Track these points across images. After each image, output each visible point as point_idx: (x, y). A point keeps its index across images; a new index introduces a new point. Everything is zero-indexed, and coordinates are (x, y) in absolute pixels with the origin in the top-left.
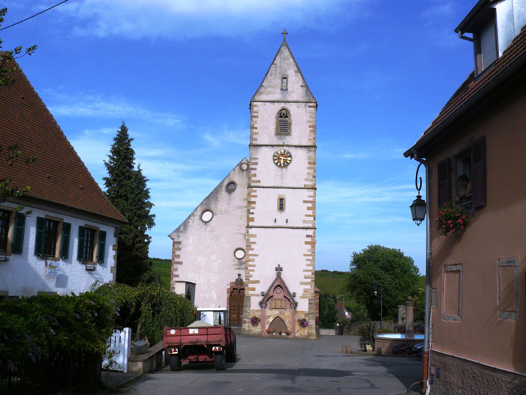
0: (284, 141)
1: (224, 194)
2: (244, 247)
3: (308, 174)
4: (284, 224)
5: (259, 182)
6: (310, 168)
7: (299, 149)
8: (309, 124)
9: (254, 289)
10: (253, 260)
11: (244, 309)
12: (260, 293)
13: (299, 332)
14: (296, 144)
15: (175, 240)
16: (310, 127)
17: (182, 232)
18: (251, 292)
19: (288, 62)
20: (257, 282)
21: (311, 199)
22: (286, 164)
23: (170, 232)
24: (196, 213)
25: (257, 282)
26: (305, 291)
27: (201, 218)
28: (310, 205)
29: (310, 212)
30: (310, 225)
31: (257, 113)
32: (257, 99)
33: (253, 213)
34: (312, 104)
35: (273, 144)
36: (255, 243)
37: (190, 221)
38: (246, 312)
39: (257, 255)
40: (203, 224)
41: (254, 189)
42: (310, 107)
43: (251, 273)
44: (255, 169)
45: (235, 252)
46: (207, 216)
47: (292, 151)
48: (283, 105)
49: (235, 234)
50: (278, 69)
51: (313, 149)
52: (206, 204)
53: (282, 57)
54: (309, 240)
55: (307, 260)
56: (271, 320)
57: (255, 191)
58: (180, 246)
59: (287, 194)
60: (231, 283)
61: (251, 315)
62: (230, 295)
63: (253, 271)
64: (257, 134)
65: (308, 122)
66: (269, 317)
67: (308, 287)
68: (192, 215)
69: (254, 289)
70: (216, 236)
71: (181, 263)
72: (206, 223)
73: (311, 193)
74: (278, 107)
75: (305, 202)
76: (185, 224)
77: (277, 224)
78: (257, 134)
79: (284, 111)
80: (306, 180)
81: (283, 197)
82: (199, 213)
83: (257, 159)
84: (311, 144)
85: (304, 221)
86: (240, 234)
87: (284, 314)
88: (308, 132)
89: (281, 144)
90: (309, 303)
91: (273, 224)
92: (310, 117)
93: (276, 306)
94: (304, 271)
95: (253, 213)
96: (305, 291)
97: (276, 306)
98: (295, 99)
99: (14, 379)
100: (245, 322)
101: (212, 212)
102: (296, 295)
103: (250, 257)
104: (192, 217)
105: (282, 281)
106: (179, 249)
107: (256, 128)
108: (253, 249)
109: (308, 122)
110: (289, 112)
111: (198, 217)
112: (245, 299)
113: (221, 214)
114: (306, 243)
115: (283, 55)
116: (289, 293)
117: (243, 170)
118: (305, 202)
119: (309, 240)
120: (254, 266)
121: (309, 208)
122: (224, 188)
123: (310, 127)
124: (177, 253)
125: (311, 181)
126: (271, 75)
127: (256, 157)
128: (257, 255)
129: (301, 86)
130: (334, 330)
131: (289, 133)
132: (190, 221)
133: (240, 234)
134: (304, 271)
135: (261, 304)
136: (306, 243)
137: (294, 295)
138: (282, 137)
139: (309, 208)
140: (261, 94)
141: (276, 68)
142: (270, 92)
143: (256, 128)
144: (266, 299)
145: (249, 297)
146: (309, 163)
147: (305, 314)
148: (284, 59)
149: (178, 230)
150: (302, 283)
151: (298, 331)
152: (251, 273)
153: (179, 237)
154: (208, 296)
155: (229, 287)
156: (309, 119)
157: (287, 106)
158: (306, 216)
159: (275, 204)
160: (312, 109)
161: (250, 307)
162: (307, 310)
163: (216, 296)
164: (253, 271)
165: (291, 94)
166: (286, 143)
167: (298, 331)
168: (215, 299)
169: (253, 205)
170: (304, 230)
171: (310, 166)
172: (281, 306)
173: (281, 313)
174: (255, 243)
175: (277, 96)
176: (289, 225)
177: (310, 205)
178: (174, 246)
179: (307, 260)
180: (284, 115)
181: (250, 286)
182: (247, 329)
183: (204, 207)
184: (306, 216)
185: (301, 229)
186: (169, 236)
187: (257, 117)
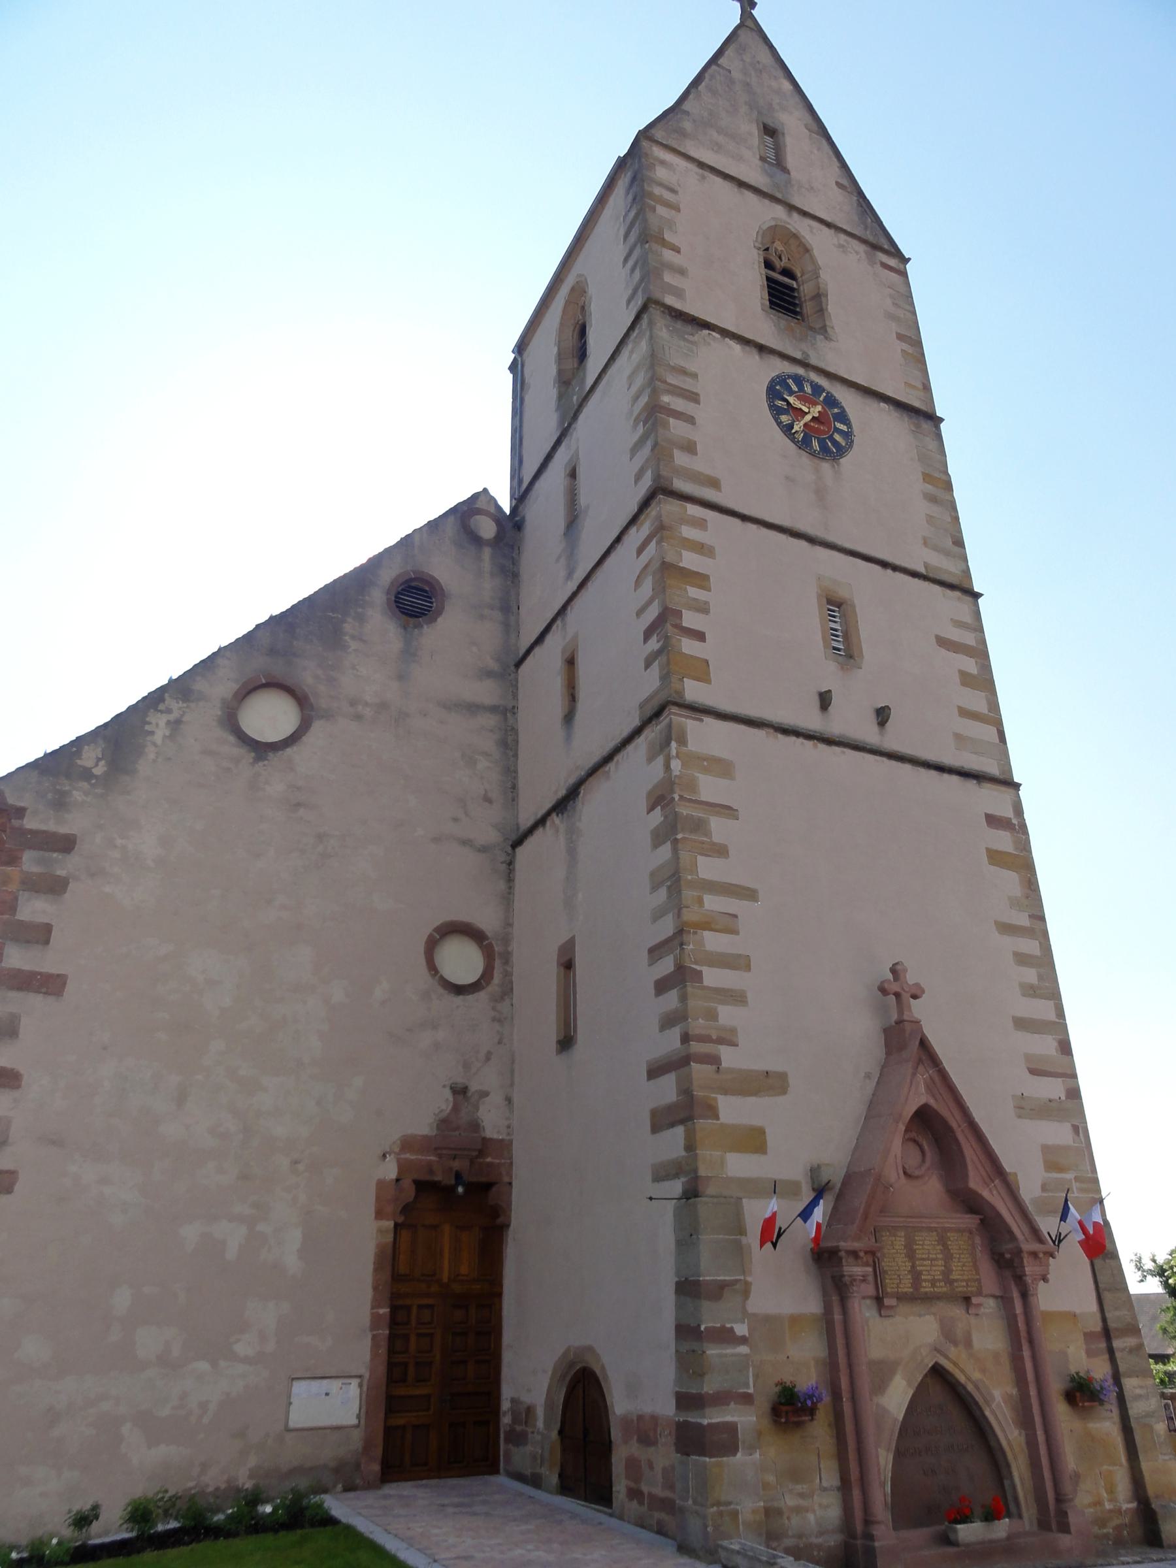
1: (378, 623)
2: (487, 919)
4: (869, 733)
9: (753, 1140)
18: (739, 1165)
20: (770, 1083)
25: (770, 1083)
27: (231, 722)
36: (728, 811)
41: (693, 510)
43: (727, 1015)
45: (431, 946)
46: (270, 717)
49: (436, 840)
52: (272, 652)
55: (41, 935)
57: (701, 524)
60: (407, 1144)
63: (737, 998)
69: (753, 1140)
70: (320, 837)
71: (51, 985)
72: (261, 750)
82: (223, 687)
86: (465, 842)
87: (968, 1343)
91: (812, 720)
101: (301, 699)
103: (713, 903)
108: (721, 851)
111: (214, 711)
113: (358, 717)
117: (476, 540)
120: (739, 963)
122: (378, 597)
127: (692, 367)
128: (750, 894)
133: (465, 842)
152: (727, 1015)
153: (60, 803)
154: (233, 1236)
155: (390, 1170)
163: (295, 1238)
164: (737, 998)
166: (813, 361)
168: (292, 1262)
169: (693, 592)
173: (947, 1332)
174: (728, 811)
176: (891, 742)
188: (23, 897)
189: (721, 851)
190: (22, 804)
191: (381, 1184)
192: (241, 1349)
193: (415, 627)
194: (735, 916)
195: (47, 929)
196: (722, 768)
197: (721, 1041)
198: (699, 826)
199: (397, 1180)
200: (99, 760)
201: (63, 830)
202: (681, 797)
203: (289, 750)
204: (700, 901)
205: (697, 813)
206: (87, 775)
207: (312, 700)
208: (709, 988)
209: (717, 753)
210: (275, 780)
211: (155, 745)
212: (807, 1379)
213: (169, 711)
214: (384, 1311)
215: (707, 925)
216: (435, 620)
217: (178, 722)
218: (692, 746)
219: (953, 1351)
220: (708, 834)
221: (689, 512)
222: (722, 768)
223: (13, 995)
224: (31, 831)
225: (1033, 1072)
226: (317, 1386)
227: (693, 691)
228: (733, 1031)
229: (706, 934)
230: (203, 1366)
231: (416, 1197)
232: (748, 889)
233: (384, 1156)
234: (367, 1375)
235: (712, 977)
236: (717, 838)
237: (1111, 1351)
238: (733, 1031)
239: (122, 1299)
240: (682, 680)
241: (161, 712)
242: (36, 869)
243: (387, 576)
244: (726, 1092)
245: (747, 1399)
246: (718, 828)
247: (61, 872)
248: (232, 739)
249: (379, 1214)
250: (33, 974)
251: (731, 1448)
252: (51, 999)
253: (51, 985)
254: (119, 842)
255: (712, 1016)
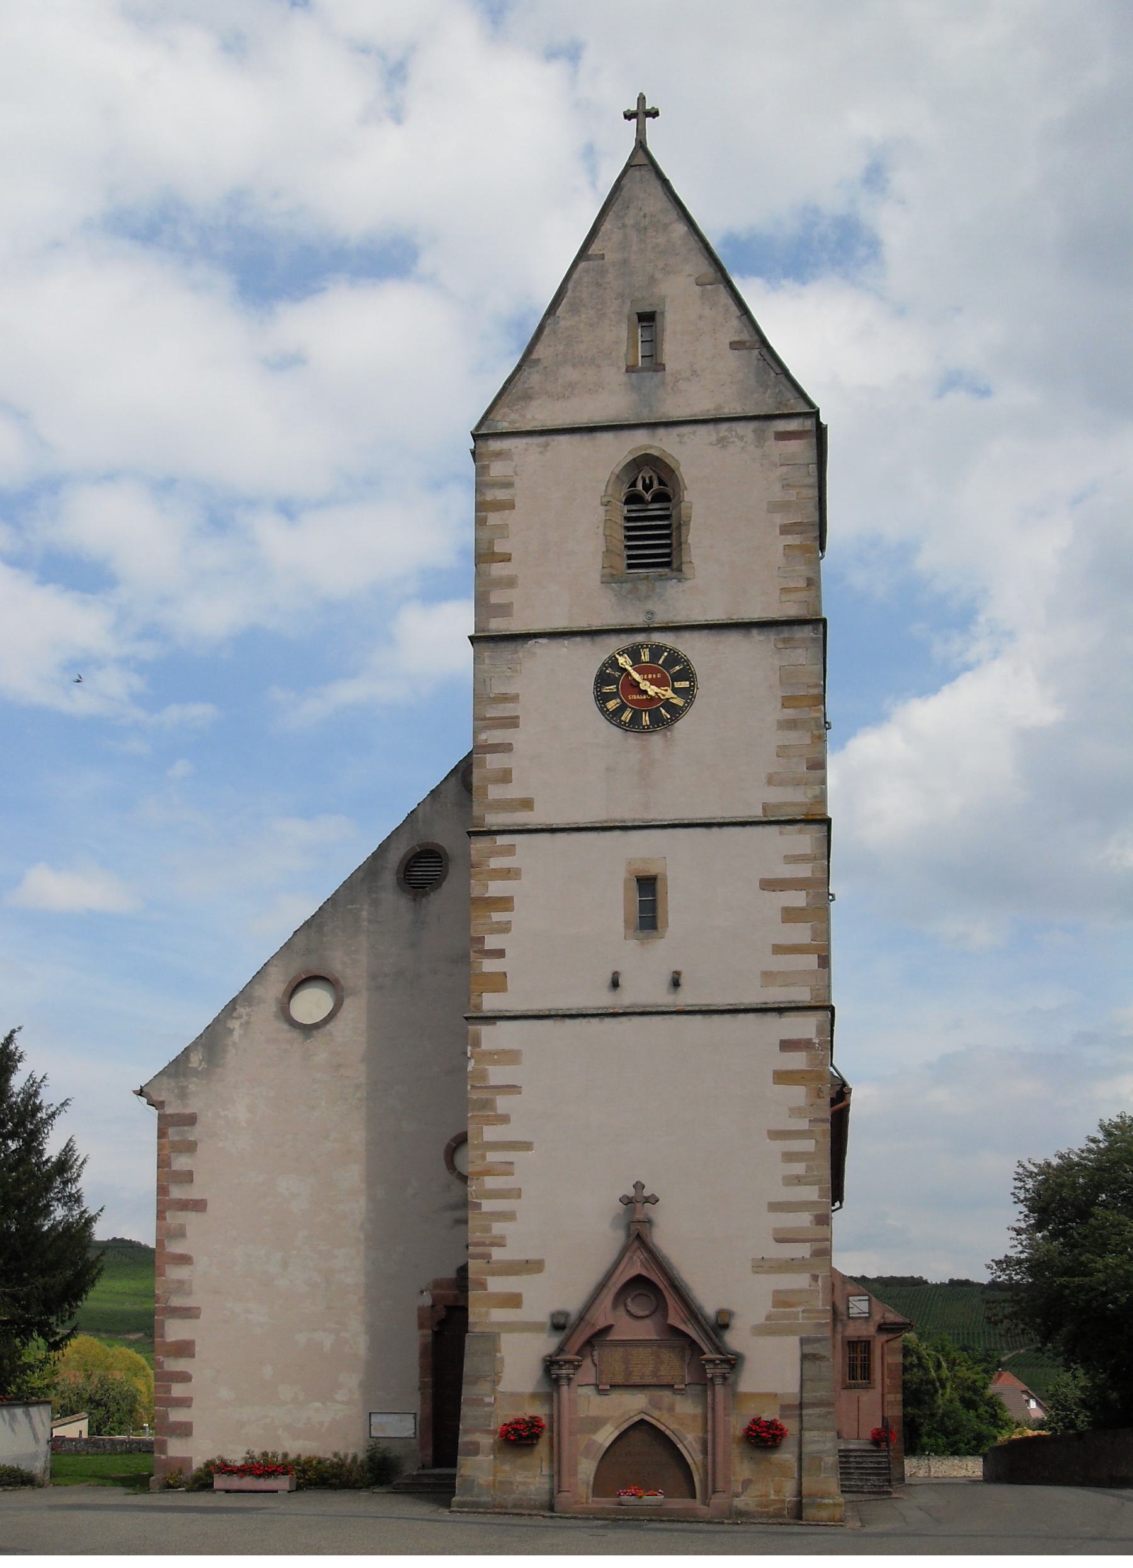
0: (650, 606)
3: (783, 751)
4: (663, 997)
5: (527, 804)
6: (790, 725)
7: (734, 638)
8: (779, 519)
10: (506, 1169)
11: (467, 1392)
12: (544, 1317)
13: (755, 1491)
14: (717, 615)
15: (169, 1110)
16: (785, 530)
17: (196, 1073)
18: (499, 1315)
19: (661, 240)
20: (532, 1266)
21: (804, 871)
22: (660, 718)
23: (144, 1077)
24: (259, 991)
25: (532, 1266)
26: (782, 1299)
28: (798, 899)
29: (801, 933)
30: (803, 995)
31: (508, 485)
32: (504, 426)
33: (500, 953)
34: (793, 425)
35: (596, 624)
36: (513, 1089)
37: (235, 1024)
38: (478, 1402)
39: (527, 1146)
40: (295, 1034)
41: (501, 840)
42: (782, 436)
43: (498, 1228)
44: (507, 748)
46: (312, 1004)
47: (691, 647)
48: (639, 441)
50: (610, 277)
51: (807, 632)
53: (629, 221)
54: (798, 1061)
55: (789, 1157)
56: (606, 1436)
57: (510, 850)
58: (193, 1134)
59: (677, 859)
60: (438, 1284)
61: (507, 1414)
62: (436, 1334)
63: (509, 1216)
64: (510, 582)
65: (775, 507)
66: (596, 1423)
67: (495, 792)
68: (245, 997)
69: (513, 1301)
71: (199, 1206)
72: (308, 1030)
73: (803, 840)
74: (618, 450)
75: (769, 885)
76: (212, 1040)
77: (627, 998)
78: (510, 582)
79: (647, 473)
80: (770, 781)
81: (652, 870)
82: (275, 988)
83: (515, 698)
84: (792, 610)
85: (768, 977)
87: (671, 1409)
88: (779, 558)
89: (639, 620)
90: (804, 1357)
91: (605, 1000)
92: (786, 486)
93: (629, 1373)
94: (776, 1207)
95: (500, 953)
96: (782, 1299)
97: (629, 1373)
98: (703, 406)
99: (814, 1442)
100: (475, 1449)
102: (736, 1323)
103: (492, 1157)
104: (241, 1010)
105: (655, 1258)
106: (190, 1147)
107: (506, 558)
108: (504, 1119)
109: (775, 507)
110: (671, 471)
112: (471, 1345)
114: (783, 1077)
115: (632, 212)
116: (692, 1312)
118: (769, 885)
119: (798, 1061)
121: (790, 915)
122: (389, 878)
123: (785, 530)
124: (181, 1163)
125: (798, 783)
126: (575, 309)
127: (511, 690)
128: (527, 1146)
129: (734, 346)
130: (980, 1461)
131: (680, 570)
132: (235, 1024)
134: (776, 1207)
135: (550, 1364)
136: (783, 1077)
137: (722, 1323)
138: (643, 587)
139: (790, 915)
140: (527, 397)
141: (603, 272)
142: (572, 386)
143: (506, 558)
144: (576, 1343)
145: (491, 1339)
146: (788, 702)
147: (784, 1408)
148: (642, 230)
149: (178, 1067)
150: (762, 1266)
151: (747, 1483)
152: (498, 1228)
153: (183, 1095)
155: (427, 1300)
156: (777, 494)
157: (664, 443)
158: (778, 949)
159: (616, 903)
160: (794, 446)
161: (496, 1382)
162: (796, 1389)
164: (509, 1216)
165: (682, 385)
166: (660, 619)
167: (747, 1483)
169: (497, 917)
170: (770, 1019)
171: (790, 713)
172: (655, 1373)
173: (655, 1404)
174: (513, 1089)
175: (611, 400)
176: (686, 998)
177: (798, 899)
178: (162, 1134)
179: (789, 1157)
180: (647, 488)
181: (497, 1285)
182: (484, 1478)
183: (297, 967)
184: (778, 949)
185: (751, 1016)
186: (141, 1093)
187: (510, 505)
188: (173, 1155)
189: (504, 1119)
190: (161, 1099)
191: (421, 1309)
192: (338, 1397)
193: (423, 896)
194: (512, 1163)
195: (190, 1174)
196: (510, 1057)
197: (492, 1245)
198: (488, 1104)
199: (433, 1306)
200: (201, 1061)
201: (187, 1111)
202: (472, 1086)
203: (328, 1027)
204: (483, 1157)
205: (485, 1095)
206: (196, 1073)
207: (342, 981)
208: (486, 1213)
209: (507, 1046)
210: (320, 1050)
211: (234, 1043)
212: (834, 1434)
213: (240, 1017)
214: (429, 1379)
215: (488, 1172)
216: (427, 894)
217: (248, 1023)
218: (485, 1046)
219: (656, 1414)
220: (494, 1109)
221: (498, 843)
222: (510, 1057)
223: (180, 1213)
224: (170, 1115)
225: (779, 1240)
226: (385, 1418)
227: (491, 1002)
228: (503, 1237)
229: (486, 1178)
230: (318, 1404)
231: (833, 1270)
232: (525, 1143)
233: (422, 1292)
234: (419, 1412)
235: (487, 1205)
236: (500, 1111)
237: (801, 1416)
238: (503, 1237)
239: (268, 1371)
240: (480, 996)
241: (236, 1018)
242: (177, 1138)
243: (395, 857)
244: (493, 1274)
245: (488, 1432)
246: (502, 1103)
247: (192, 1138)
248: (286, 1027)
249: (421, 1326)
250: (188, 1201)
251: (476, 1453)
252: (199, 1214)
253: (199, 1206)
254: (222, 1113)
255: (488, 1229)
